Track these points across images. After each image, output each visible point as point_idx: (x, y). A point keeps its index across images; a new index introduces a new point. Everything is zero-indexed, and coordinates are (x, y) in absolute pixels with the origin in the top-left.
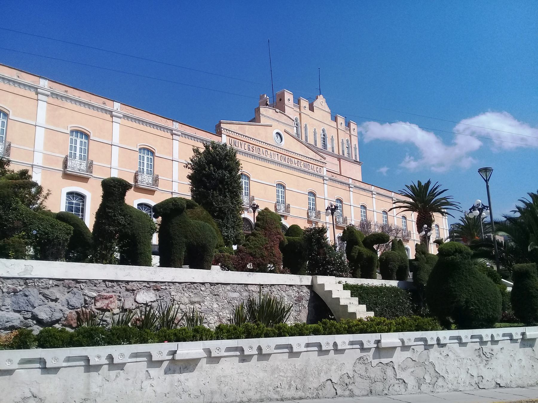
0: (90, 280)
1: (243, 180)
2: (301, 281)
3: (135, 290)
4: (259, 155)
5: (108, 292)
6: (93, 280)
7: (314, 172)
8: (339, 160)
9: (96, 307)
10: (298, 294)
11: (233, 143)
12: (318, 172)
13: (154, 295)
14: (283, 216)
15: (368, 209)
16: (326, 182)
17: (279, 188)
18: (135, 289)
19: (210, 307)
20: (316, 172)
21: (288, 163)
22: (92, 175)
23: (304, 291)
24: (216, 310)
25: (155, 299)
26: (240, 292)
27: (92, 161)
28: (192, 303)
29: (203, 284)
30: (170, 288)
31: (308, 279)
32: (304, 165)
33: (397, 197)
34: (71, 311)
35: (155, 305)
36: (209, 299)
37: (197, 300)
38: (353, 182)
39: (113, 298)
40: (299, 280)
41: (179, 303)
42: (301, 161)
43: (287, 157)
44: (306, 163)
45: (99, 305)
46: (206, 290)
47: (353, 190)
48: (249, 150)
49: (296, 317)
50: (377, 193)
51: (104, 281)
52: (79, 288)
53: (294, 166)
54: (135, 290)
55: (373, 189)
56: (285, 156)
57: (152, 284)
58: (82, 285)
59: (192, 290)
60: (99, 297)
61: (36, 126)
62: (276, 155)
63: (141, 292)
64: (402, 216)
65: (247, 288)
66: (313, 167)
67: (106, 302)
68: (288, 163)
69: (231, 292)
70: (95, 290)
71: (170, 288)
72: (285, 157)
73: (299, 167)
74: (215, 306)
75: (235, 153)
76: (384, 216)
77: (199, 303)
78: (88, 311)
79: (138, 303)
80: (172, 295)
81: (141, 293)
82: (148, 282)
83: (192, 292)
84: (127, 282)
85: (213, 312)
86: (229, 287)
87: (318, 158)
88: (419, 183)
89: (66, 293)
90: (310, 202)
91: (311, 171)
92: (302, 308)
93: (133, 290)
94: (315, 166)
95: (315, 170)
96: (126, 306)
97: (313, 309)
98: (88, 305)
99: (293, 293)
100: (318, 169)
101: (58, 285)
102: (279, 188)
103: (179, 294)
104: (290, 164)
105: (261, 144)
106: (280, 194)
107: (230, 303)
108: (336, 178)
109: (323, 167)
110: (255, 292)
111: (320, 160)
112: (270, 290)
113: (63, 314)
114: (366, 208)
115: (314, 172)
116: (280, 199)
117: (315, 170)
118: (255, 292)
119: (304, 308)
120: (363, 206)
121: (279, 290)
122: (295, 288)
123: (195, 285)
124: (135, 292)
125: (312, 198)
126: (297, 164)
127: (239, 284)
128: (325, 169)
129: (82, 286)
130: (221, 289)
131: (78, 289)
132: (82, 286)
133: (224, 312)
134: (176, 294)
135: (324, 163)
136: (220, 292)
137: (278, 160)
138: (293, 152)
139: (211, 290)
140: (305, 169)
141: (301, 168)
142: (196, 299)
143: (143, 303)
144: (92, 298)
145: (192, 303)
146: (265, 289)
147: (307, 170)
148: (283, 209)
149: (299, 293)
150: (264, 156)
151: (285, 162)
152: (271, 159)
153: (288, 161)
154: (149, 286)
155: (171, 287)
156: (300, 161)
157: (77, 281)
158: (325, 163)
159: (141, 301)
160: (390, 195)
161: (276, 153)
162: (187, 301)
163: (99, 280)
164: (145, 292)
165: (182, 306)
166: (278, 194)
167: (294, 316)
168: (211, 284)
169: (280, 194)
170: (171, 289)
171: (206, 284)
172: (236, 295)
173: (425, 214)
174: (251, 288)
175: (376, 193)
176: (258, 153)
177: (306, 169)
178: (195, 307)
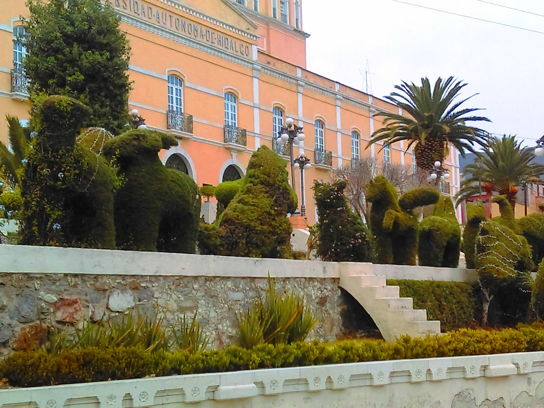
0: (46, 275)
1: (174, 85)
2: (325, 271)
3: (107, 290)
4: (136, 15)
5: (71, 294)
6: (51, 275)
7: (236, 53)
8: (267, 25)
9: (56, 319)
10: (320, 292)
11: (229, 45)
12: (243, 55)
13: (132, 297)
14: (181, 138)
15: (187, 84)
16: (257, 75)
17: (229, 101)
18: (107, 288)
19: (206, 316)
20: (239, 54)
21: (190, 34)
22: (192, 136)
23: (329, 288)
24: (213, 320)
25: (133, 305)
26: (244, 290)
27: (191, 116)
28: (182, 310)
29: (196, 278)
30: (153, 286)
31: (334, 268)
32: (219, 39)
33: (377, 105)
34: (24, 326)
35: (134, 313)
36: (204, 303)
37: (188, 305)
38: (304, 75)
39: (77, 304)
40: (322, 269)
41: (165, 310)
42: (213, 31)
43: (187, 22)
44: (222, 35)
45: (60, 315)
46: (200, 289)
47: (303, 91)
48: (117, 4)
49: (319, 330)
50: (262, 67)
51: (66, 275)
52: (31, 288)
53: (200, 40)
54: (107, 290)
55: (337, 90)
56: (184, 19)
57: (129, 280)
58: (37, 283)
59: (182, 289)
60: (60, 303)
61: (337, 132)
62: (168, 18)
63: (114, 293)
64: (353, 132)
65: (254, 284)
66: (164, 14)
67: (71, 310)
68: (190, 34)
69: (234, 291)
70: (54, 291)
71: (153, 286)
72: (183, 21)
73: (210, 44)
74: (213, 314)
75: (117, 21)
76: (354, 141)
77: (190, 309)
78: (46, 326)
79: (111, 311)
80: (155, 297)
81: (115, 295)
82: (124, 277)
83: (182, 292)
84: (96, 277)
85: (210, 325)
86: (229, 284)
87: (244, 26)
88: (425, 82)
89: (14, 297)
90: (172, 97)
91: (231, 51)
92: (326, 315)
93: (105, 290)
94: (238, 43)
95: (238, 49)
96: (97, 318)
97: (340, 318)
98: (46, 316)
99: (315, 293)
100: (244, 49)
101: (4, 283)
102: (229, 101)
103: (165, 296)
104: (194, 37)
105: (178, 10)
106: (174, 96)
107: (231, 308)
108: (273, 66)
109: (251, 44)
110: (264, 290)
111: (248, 31)
112: (283, 287)
113: (13, 331)
114: (237, 97)
115: (236, 53)
116: (175, 105)
117: (238, 49)
118: (264, 290)
119: (328, 315)
120: (279, 108)
121: (295, 287)
122: (316, 283)
123: (186, 280)
124: (108, 293)
125: (231, 105)
126: (205, 38)
127: (244, 278)
128: (255, 49)
129: (36, 284)
130: (219, 287)
131: (31, 289)
132: (36, 284)
133: (224, 325)
134: (160, 295)
135: (254, 36)
136: (219, 291)
137: (171, 28)
138: (200, 11)
139: (206, 288)
140: (220, 48)
141: (213, 45)
142: (188, 304)
143: (118, 312)
144: (51, 304)
145: (182, 310)
146: (277, 284)
147: (146, 19)
148: (180, 125)
149: (322, 291)
150: (146, 19)
151: (183, 33)
152: (159, 24)
153: (190, 32)
154: (125, 283)
155: (154, 285)
156: (211, 31)
157: (29, 276)
158: (255, 36)
159: (115, 308)
160: (366, 101)
161: (168, 14)
162: (175, 306)
163: (59, 275)
164: (120, 293)
165: (169, 316)
166: (170, 95)
167: (315, 329)
168: (207, 279)
169: (174, 96)
170: (153, 288)
171: (199, 279)
172: (239, 296)
173: (433, 142)
174: (258, 285)
175: (260, 68)
176: (226, 47)
177: (222, 48)
178: (186, 317)
